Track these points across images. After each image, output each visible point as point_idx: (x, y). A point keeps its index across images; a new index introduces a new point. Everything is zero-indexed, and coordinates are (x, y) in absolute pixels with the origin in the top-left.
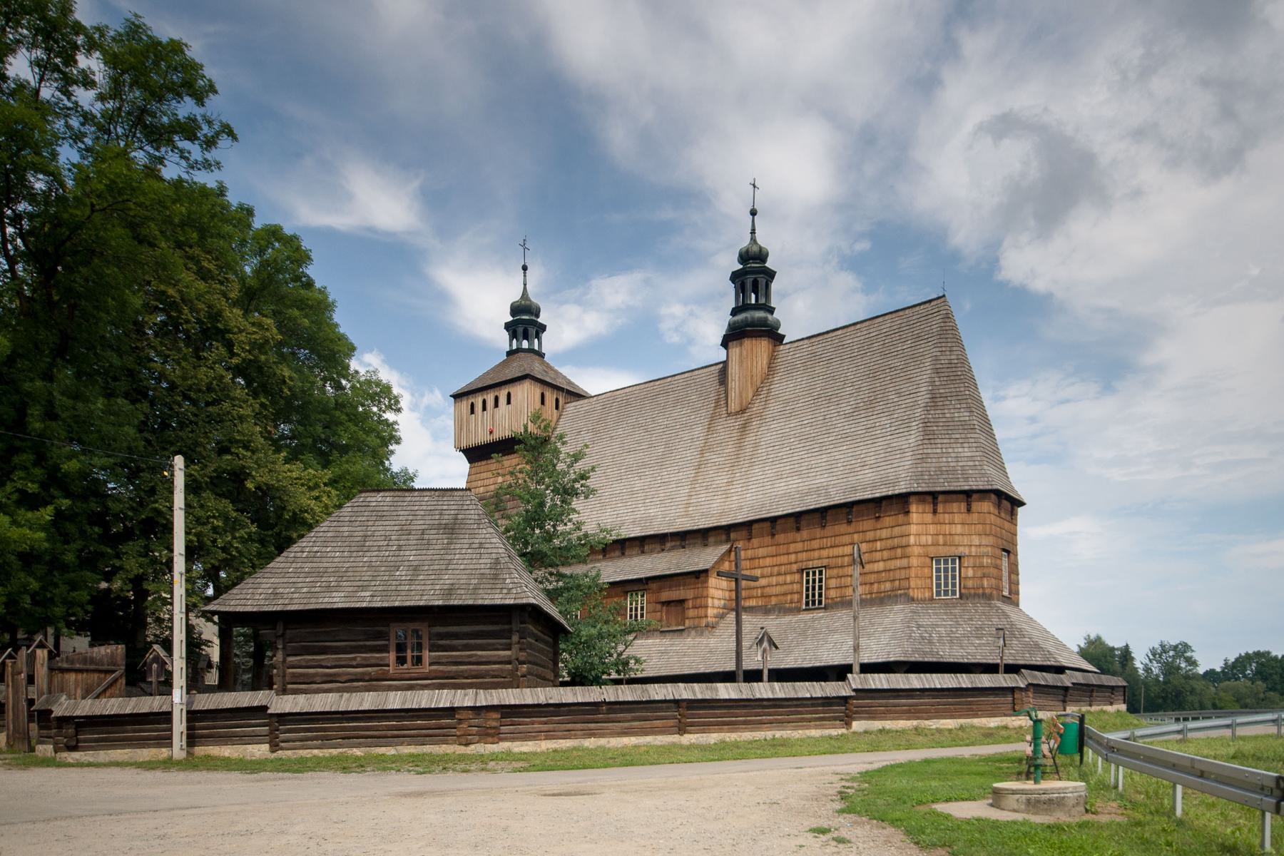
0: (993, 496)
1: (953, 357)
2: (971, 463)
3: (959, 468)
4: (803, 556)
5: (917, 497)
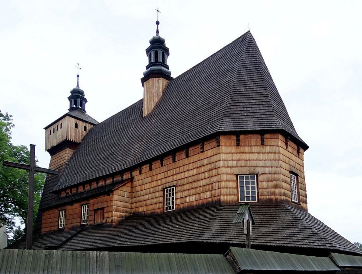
0: (280, 137)
4: (164, 181)
5: (225, 137)
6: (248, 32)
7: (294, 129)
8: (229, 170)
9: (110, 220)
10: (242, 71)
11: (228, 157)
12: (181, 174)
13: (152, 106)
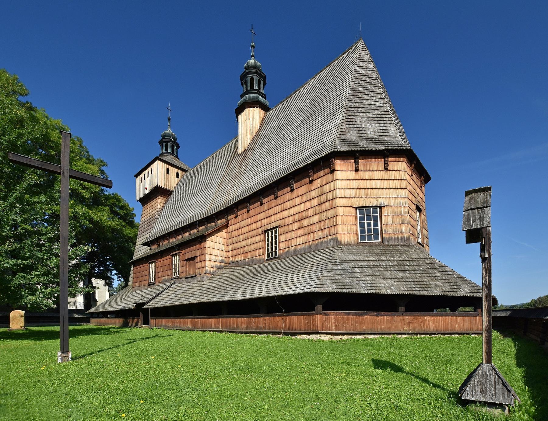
1: (368, 69)
2: (387, 134)
3: (377, 137)
4: (265, 222)
11: (344, 184)
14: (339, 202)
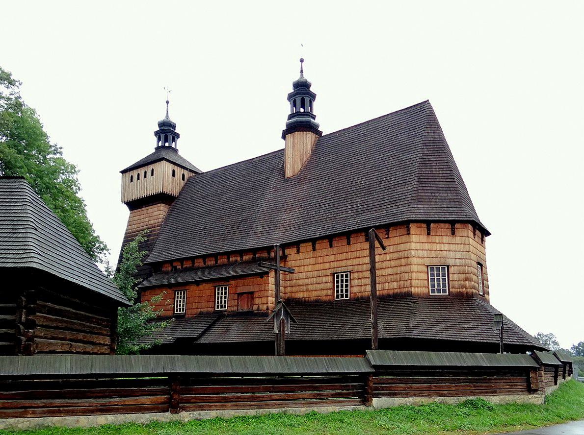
0: (470, 226)
4: (335, 264)
5: (415, 225)
6: (426, 101)
7: (474, 211)
8: (420, 261)
9: (265, 307)
10: (425, 150)
12: (358, 259)
13: (299, 166)
14: (414, 260)
